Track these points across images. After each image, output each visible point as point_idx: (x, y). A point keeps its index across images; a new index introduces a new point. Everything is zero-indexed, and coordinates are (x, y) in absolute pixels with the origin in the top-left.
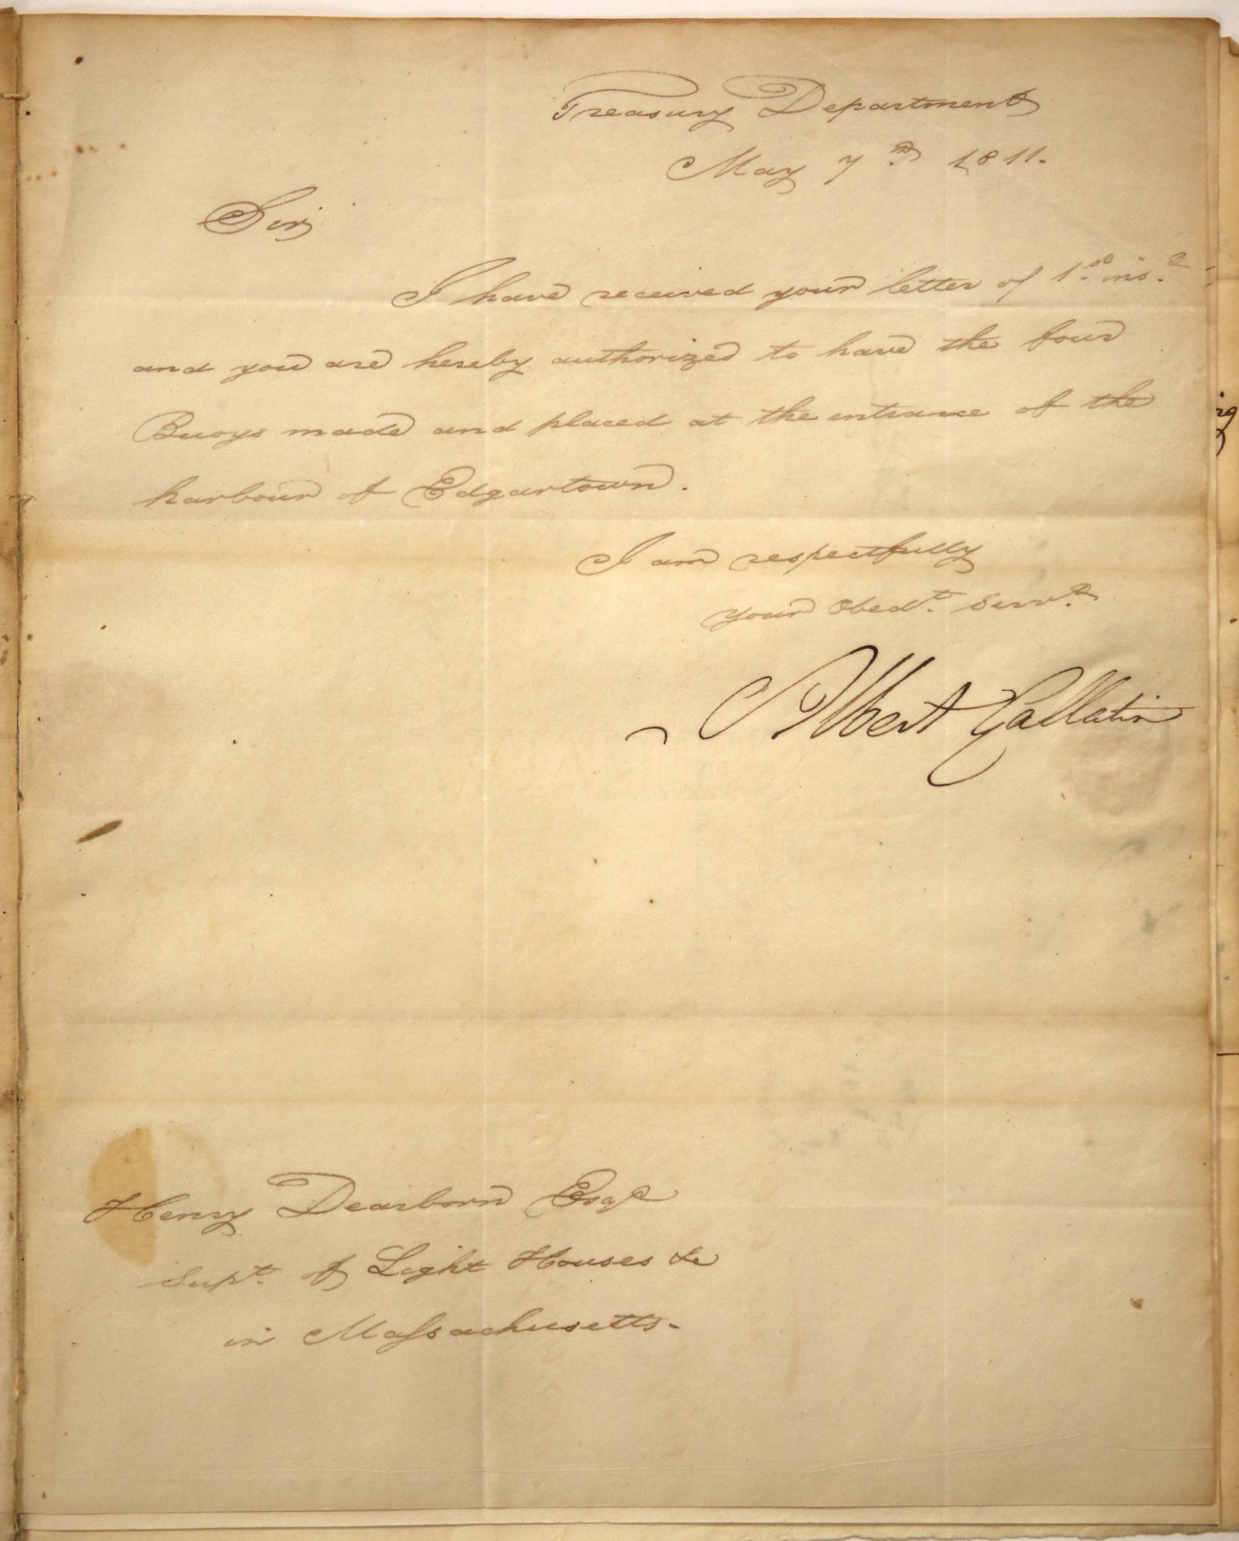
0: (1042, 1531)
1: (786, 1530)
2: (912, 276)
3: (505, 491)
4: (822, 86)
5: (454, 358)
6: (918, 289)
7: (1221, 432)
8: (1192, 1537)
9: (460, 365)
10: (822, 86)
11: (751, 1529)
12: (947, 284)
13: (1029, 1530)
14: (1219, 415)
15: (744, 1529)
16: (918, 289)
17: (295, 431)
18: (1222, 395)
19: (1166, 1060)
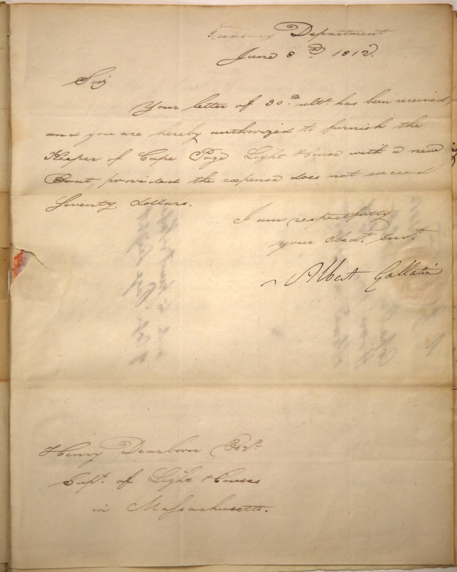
0: (388, 567)
1: (293, 567)
2: (202, 102)
3: (68, 136)
4: (311, 26)
5: (378, 99)
6: (205, 107)
7: (454, 157)
8: (444, 569)
9: (379, 102)
10: (311, 26)
11: (280, 567)
12: (216, 105)
13: (384, 567)
14: (453, 151)
15: (278, 567)
16: (205, 107)
17: (414, 151)
18: (454, 144)
19: (449, 391)
